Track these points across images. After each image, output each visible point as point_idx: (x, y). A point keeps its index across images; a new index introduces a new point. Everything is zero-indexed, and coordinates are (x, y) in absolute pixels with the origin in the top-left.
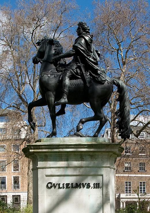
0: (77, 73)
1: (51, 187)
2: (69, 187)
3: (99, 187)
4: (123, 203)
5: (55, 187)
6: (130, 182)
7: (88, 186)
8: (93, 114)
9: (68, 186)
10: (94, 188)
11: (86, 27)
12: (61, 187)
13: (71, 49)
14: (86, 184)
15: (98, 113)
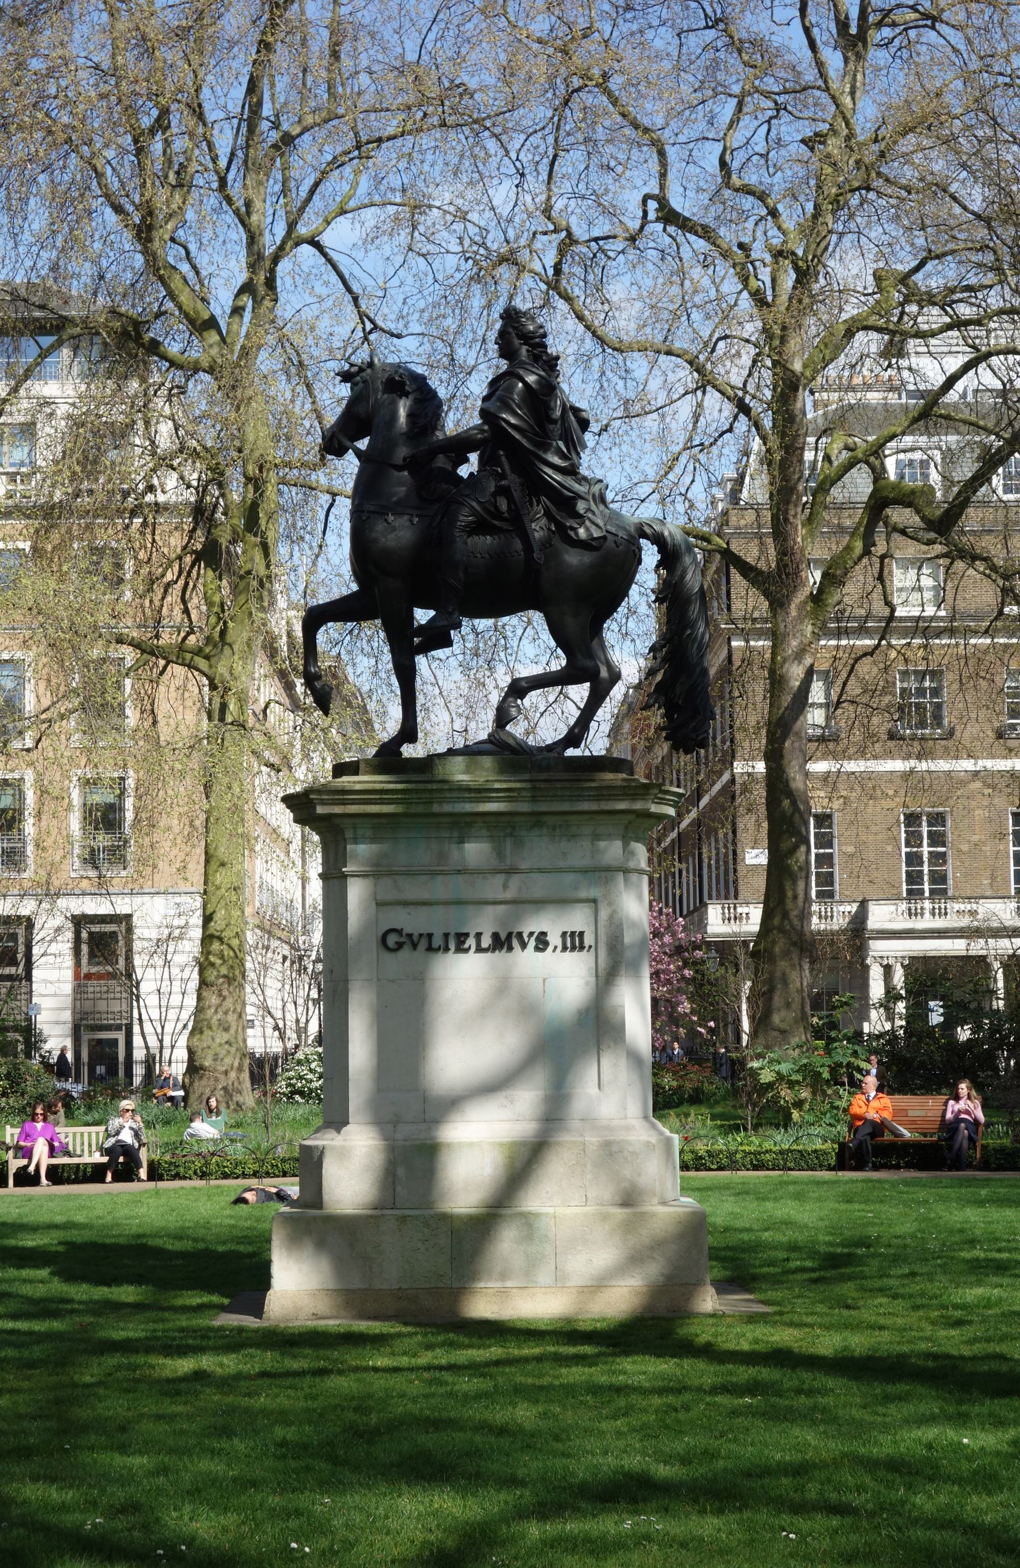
0: (497, 514)
1: (400, 946)
2: (466, 946)
3: (582, 948)
4: (888, 970)
5: (415, 946)
6: (937, 819)
7: (542, 943)
8: (559, 663)
9: (464, 942)
10: (564, 948)
11: (531, 328)
12: (435, 945)
13: (477, 421)
14: (531, 934)
15: (580, 657)
